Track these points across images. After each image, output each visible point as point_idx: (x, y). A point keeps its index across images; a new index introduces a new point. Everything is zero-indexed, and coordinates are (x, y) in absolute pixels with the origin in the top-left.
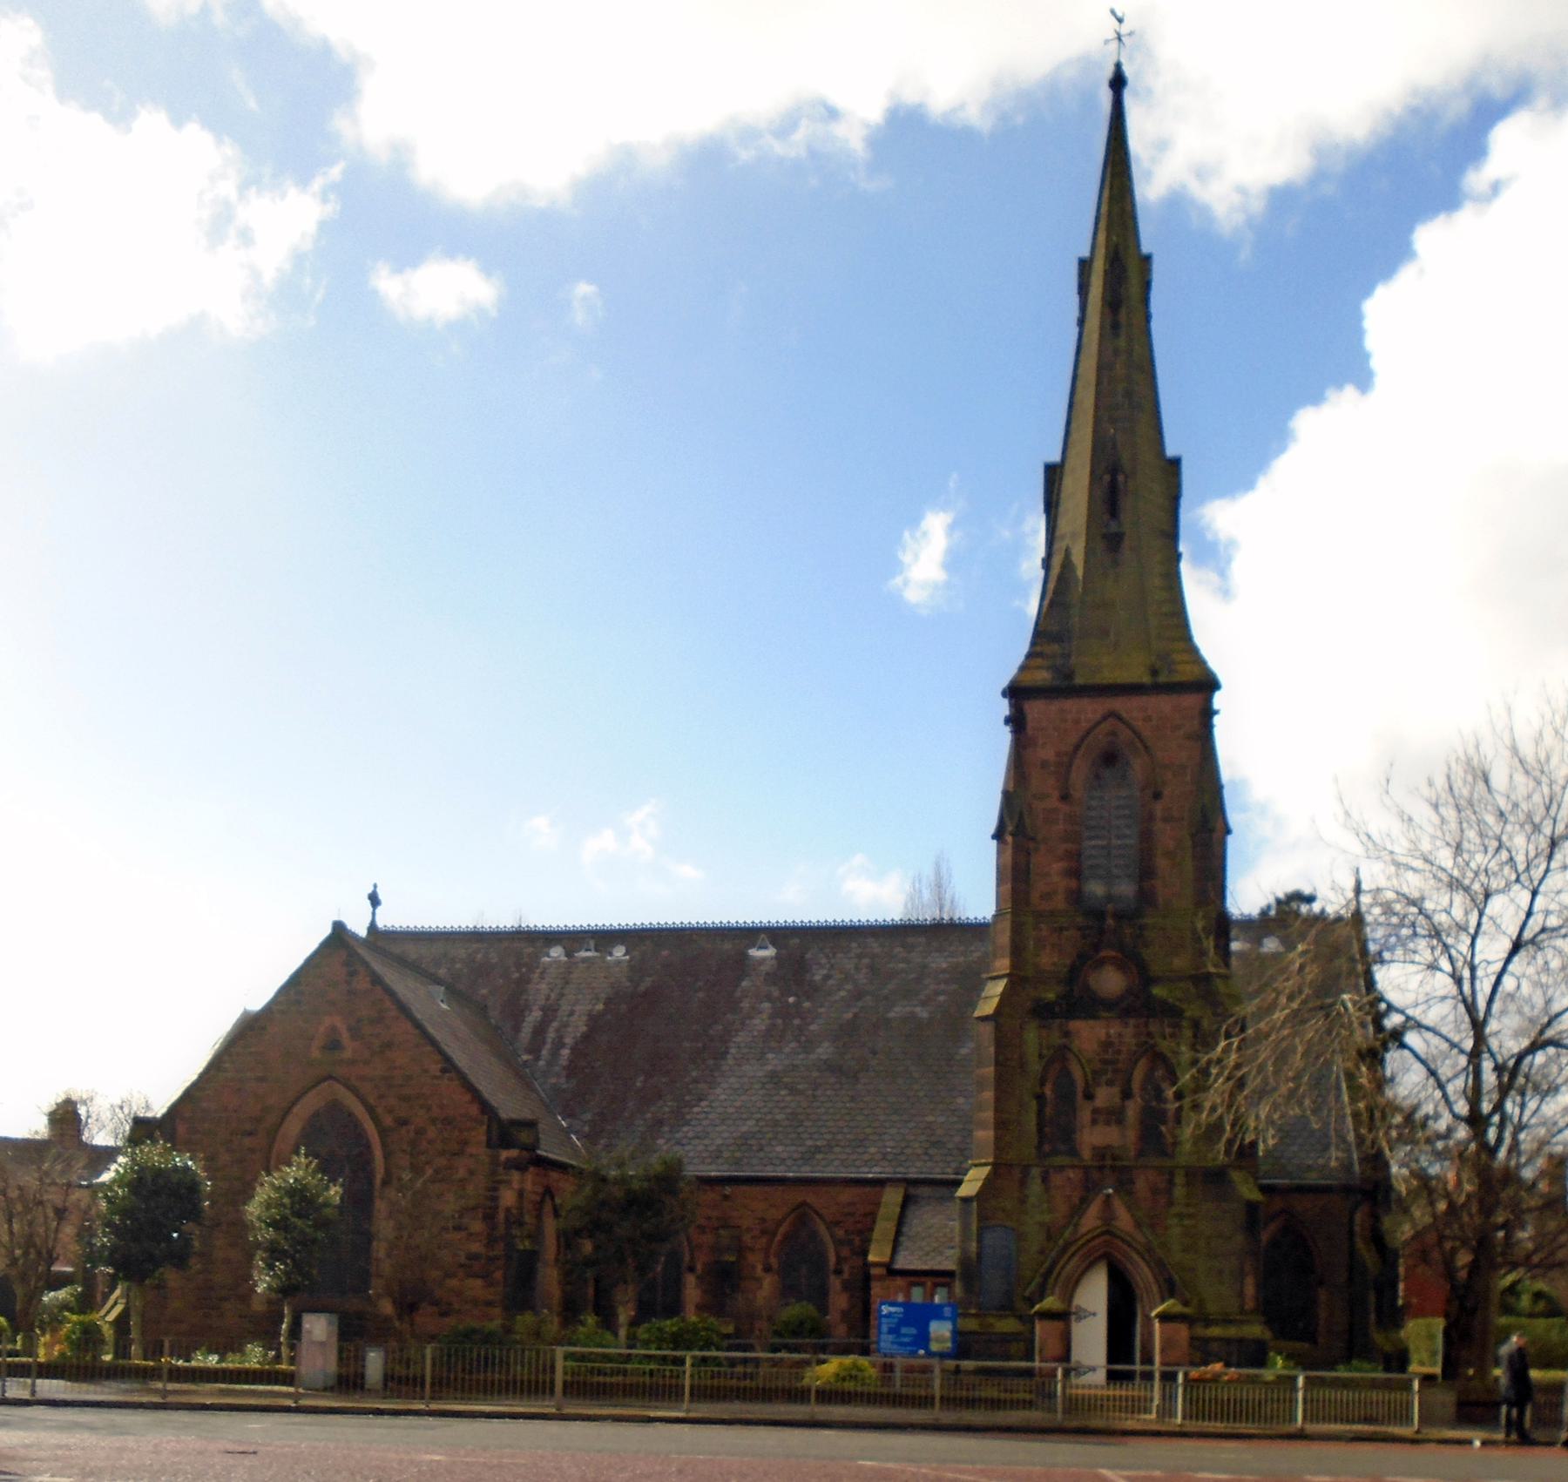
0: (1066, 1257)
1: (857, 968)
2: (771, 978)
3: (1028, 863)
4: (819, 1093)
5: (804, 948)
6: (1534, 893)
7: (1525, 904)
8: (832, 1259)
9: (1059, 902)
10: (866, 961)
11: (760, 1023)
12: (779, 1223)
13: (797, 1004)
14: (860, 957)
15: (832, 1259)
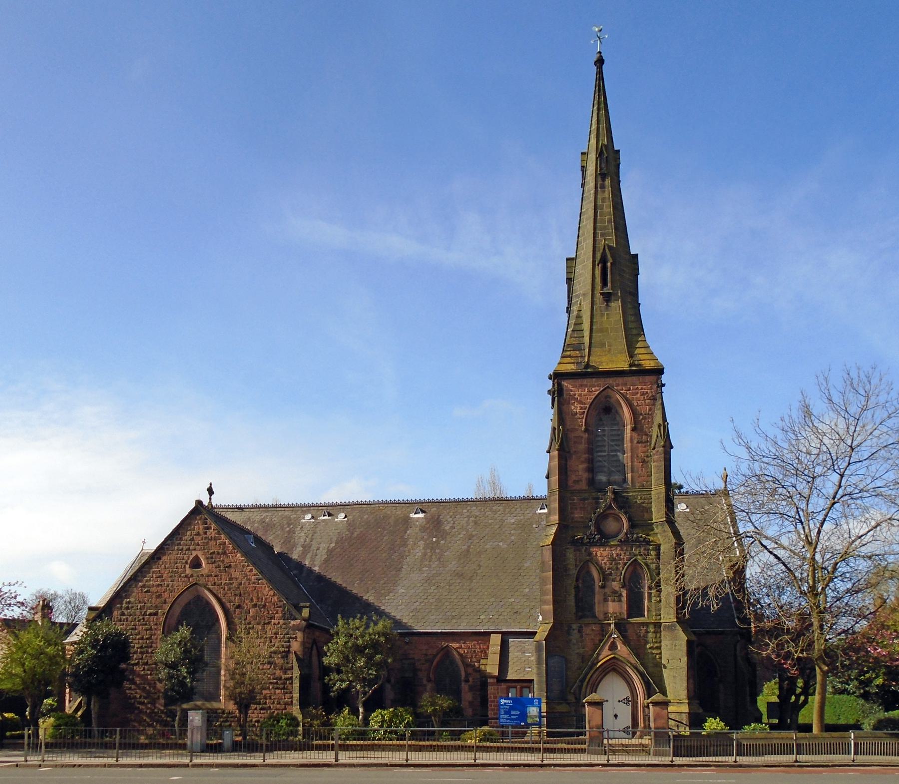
0: (592, 671)
1: (467, 522)
2: (423, 529)
3: (566, 465)
4: (452, 587)
5: (438, 513)
6: (842, 476)
7: (836, 481)
8: (463, 674)
9: (583, 485)
10: (473, 519)
11: (418, 553)
12: (435, 656)
13: (438, 542)
14: (469, 517)
15: (463, 674)
